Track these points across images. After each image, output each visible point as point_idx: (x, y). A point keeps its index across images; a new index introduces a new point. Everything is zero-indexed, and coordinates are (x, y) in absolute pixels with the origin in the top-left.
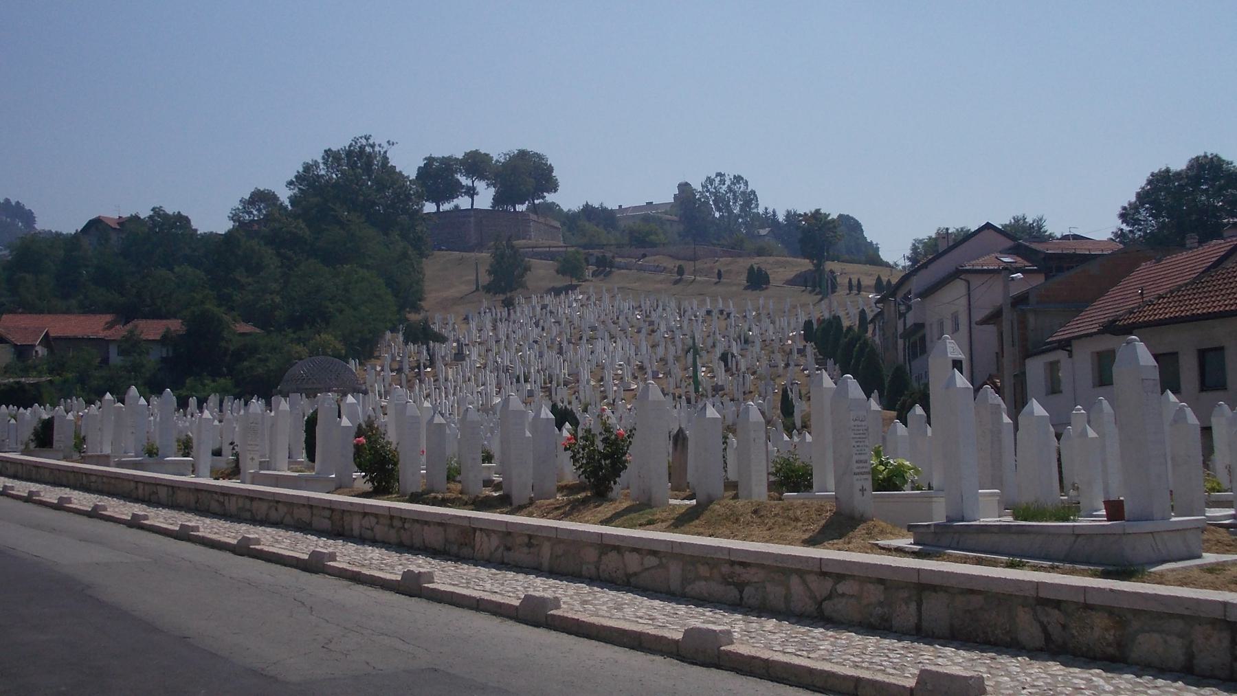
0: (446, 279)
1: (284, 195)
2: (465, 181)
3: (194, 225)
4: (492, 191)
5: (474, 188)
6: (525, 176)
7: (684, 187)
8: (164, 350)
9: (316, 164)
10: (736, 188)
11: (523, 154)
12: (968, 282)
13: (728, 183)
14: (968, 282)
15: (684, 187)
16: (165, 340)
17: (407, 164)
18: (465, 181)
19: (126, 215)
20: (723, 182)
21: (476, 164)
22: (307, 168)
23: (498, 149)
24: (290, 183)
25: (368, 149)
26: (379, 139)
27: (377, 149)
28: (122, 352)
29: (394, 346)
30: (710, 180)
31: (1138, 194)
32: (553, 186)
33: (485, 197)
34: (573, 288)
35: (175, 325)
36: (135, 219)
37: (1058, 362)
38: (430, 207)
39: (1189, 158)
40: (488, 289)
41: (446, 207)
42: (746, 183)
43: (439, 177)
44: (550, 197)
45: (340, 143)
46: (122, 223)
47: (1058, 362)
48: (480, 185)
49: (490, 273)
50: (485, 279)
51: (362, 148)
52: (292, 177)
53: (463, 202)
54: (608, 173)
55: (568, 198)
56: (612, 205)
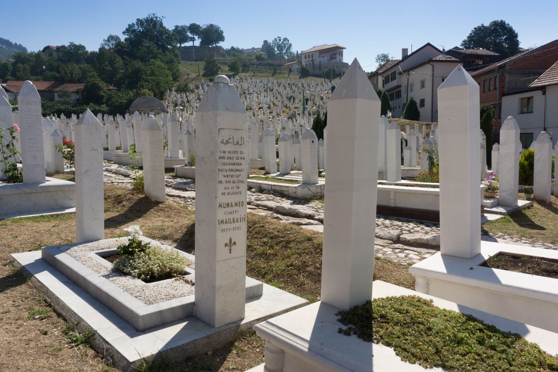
0: (189, 70)
1: (123, 38)
2: (190, 35)
3: (87, 49)
4: (200, 40)
5: (194, 38)
6: (212, 35)
7: (266, 42)
8: (78, 96)
9: (133, 24)
10: (285, 43)
11: (212, 26)
12: (433, 66)
13: (282, 40)
14: (433, 66)
15: (266, 42)
16: (77, 92)
17: (169, 25)
18: (190, 35)
19: (59, 45)
20: (280, 40)
21: (194, 28)
22: (130, 26)
23: (203, 23)
24: (124, 33)
25: (154, 19)
26: (159, 15)
27: (158, 19)
28: (60, 96)
29: (173, 96)
30: (276, 40)
31: (468, 37)
32: (222, 38)
33: (197, 42)
34: (236, 75)
35: (81, 86)
36: (63, 47)
37: (532, 97)
38: (178, 45)
39: (491, 22)
40: (204, 75)
41: (183, 45)
42: (288, 41)
43: (180, 34)
44: (221, 44)
45: (143, 16)
46: (58, 49)
47: (532, 97)
48: (196, 37)
49: (204, 69)
50: (202, 72)
51: (152, 19)
52: (124, 30)
53: (189, 44)
54: (242, 36)
55: (225, 45)
56: (241, 48)
